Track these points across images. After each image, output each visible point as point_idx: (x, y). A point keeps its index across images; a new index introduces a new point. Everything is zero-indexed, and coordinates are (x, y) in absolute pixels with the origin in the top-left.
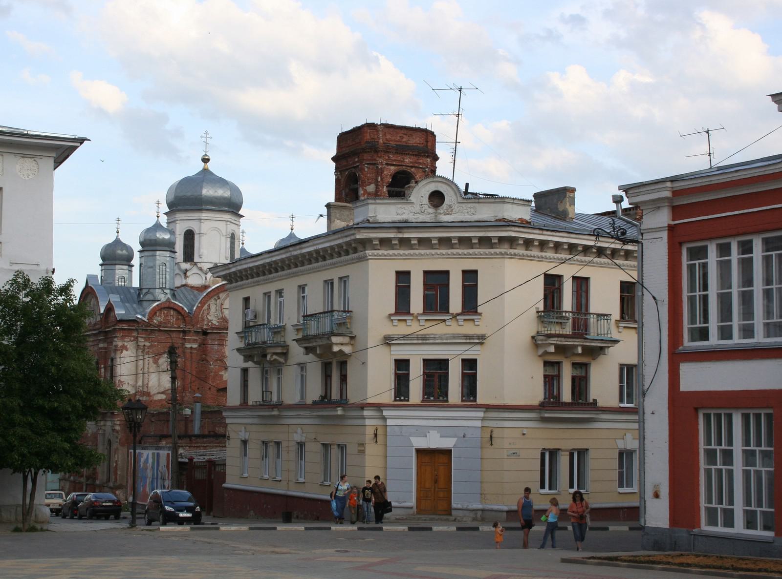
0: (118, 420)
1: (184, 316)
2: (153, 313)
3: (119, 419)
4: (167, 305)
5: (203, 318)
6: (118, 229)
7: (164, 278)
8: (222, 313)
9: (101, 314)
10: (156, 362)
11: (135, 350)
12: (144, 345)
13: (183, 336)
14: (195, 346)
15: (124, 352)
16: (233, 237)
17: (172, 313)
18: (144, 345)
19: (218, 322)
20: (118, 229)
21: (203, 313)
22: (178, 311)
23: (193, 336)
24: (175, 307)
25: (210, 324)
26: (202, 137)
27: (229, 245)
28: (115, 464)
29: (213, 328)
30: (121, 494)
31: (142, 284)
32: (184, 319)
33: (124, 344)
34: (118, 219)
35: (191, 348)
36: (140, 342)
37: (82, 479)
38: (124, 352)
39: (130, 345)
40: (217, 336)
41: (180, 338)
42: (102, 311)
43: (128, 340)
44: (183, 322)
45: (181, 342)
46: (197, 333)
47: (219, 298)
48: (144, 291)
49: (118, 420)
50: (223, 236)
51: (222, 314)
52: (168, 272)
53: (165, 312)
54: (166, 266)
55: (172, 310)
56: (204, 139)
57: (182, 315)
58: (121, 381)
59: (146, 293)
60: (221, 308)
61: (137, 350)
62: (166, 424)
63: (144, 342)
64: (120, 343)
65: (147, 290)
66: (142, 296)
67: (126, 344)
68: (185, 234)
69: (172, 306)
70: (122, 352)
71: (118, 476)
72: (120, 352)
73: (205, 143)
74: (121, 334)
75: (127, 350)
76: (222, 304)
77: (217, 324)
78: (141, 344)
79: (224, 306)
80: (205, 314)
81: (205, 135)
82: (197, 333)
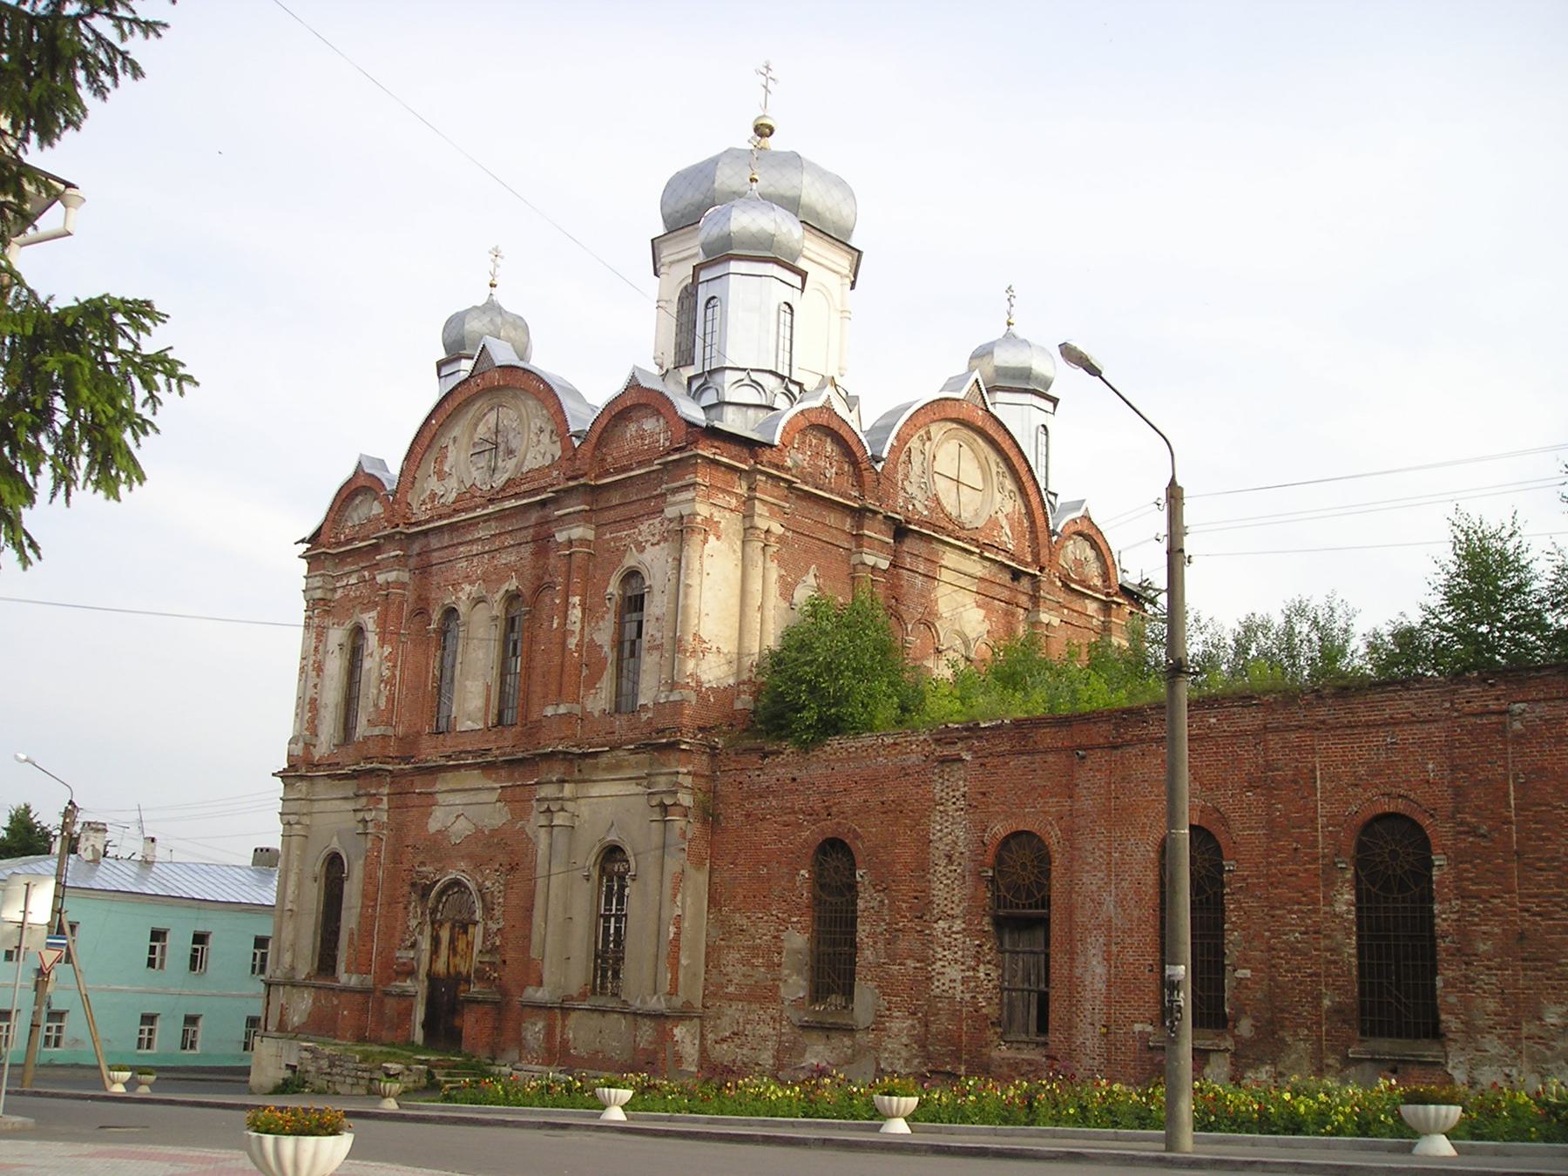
3: (690, 768)
23: (880, 532)
29: (920, 523)
49: (689, 773)
69: (835, 425)
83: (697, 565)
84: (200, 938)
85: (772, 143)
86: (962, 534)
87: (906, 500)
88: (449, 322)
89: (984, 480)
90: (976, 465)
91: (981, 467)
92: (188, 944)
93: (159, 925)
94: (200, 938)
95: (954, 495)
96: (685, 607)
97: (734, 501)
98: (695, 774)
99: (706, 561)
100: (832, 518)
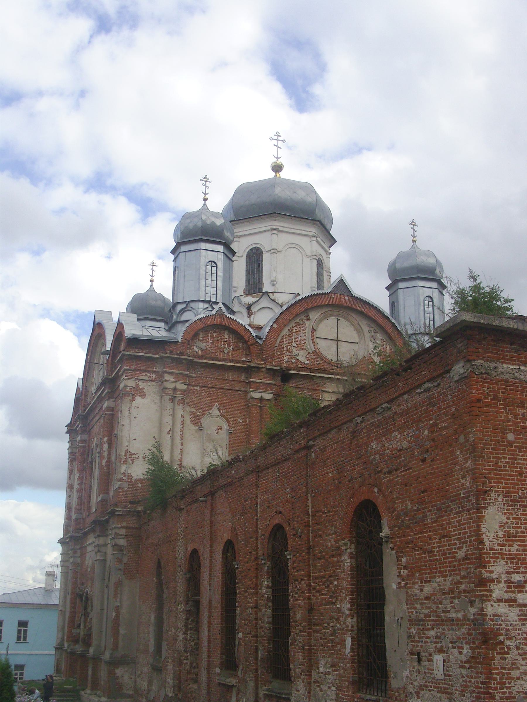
0: (123, 527)
1: (249, 343)
2: (193, 333)
3: (124, 524)
4: (218, 321)
5: (281, 348)
6: (152, 276)
7: (214, 283)
8: (315, 344)
9: (106, 353)
10: (196, 420)
11: (158, 398)
12: (175, 389)
13: (247, 378)
14: (268, 396)
15: (138, 399)
16: (320, 264)
17: (226, 336)
18: (175, 389)
19: (308, 359)
20: (152, 276)
21: (282, 341)
22: (238, 334)
23: (265, 378)
24: (231, 326)
25: (294, 361)
26: (271, 139)
27: (315, 270)
28: (114, 614)
29: (298, 369)
30: (126, 677)
31: (176, 292)
32: (248, 348)
33: (137, 385)
34: (153, 263)
35: (261, 399)
36: (168, 381)
37: (77, 646)
38: (138, 399)
39: (150, 388)
40: (307, 384)
41: (240, 381)
42: (108, 348)
43: (147, 378)
44: (246, 355)
45: (242, 389)
46: (272, 372)
47: (308, 319)
48: (179, 307)
49: (123, 527)
50: (307, 256)
51: (314, 345)
52: (220, 276)
53: (215, 335)
54: (217, 267)
55: (226, 332)
56: (275, 142)
57: (246, 342)
58: (130, 452)
59: (183, 311)
60: (313, 337)
61: (162, 397)
62: (209, 503)
63: (175, 382)
64: (131, 383)
65: (184, 306)
66: (175, 317)
67: (141, 384)
68: (248, 256)
69: (226, 323)
70: (133, 400)
71: (120, 638)
72: (130, 398)
73: (276, 147)
74: (134, 367)
75: (143, 396)
76: (314, 330)
77: (307, 362)
78: (171, 386)
79: (318, 334)
80: (285, 344)
81: (276, 138)
82: (272, 372)
83: (127, 413)
84: (23, 624)
85: (283, 175)
86: (341, 371)
87: (291, 357)
88: (389, 268)
89: (359, 336)
90: (352, 328)
91: (356, 329)
92: (15, 628)
93: (23, 619)
94: (23, 624)
95: (335, 349)
96: (116, 436)
97: (154, 375)
98: (126, 528)
99: (134, 412)
100: (230, 376)
